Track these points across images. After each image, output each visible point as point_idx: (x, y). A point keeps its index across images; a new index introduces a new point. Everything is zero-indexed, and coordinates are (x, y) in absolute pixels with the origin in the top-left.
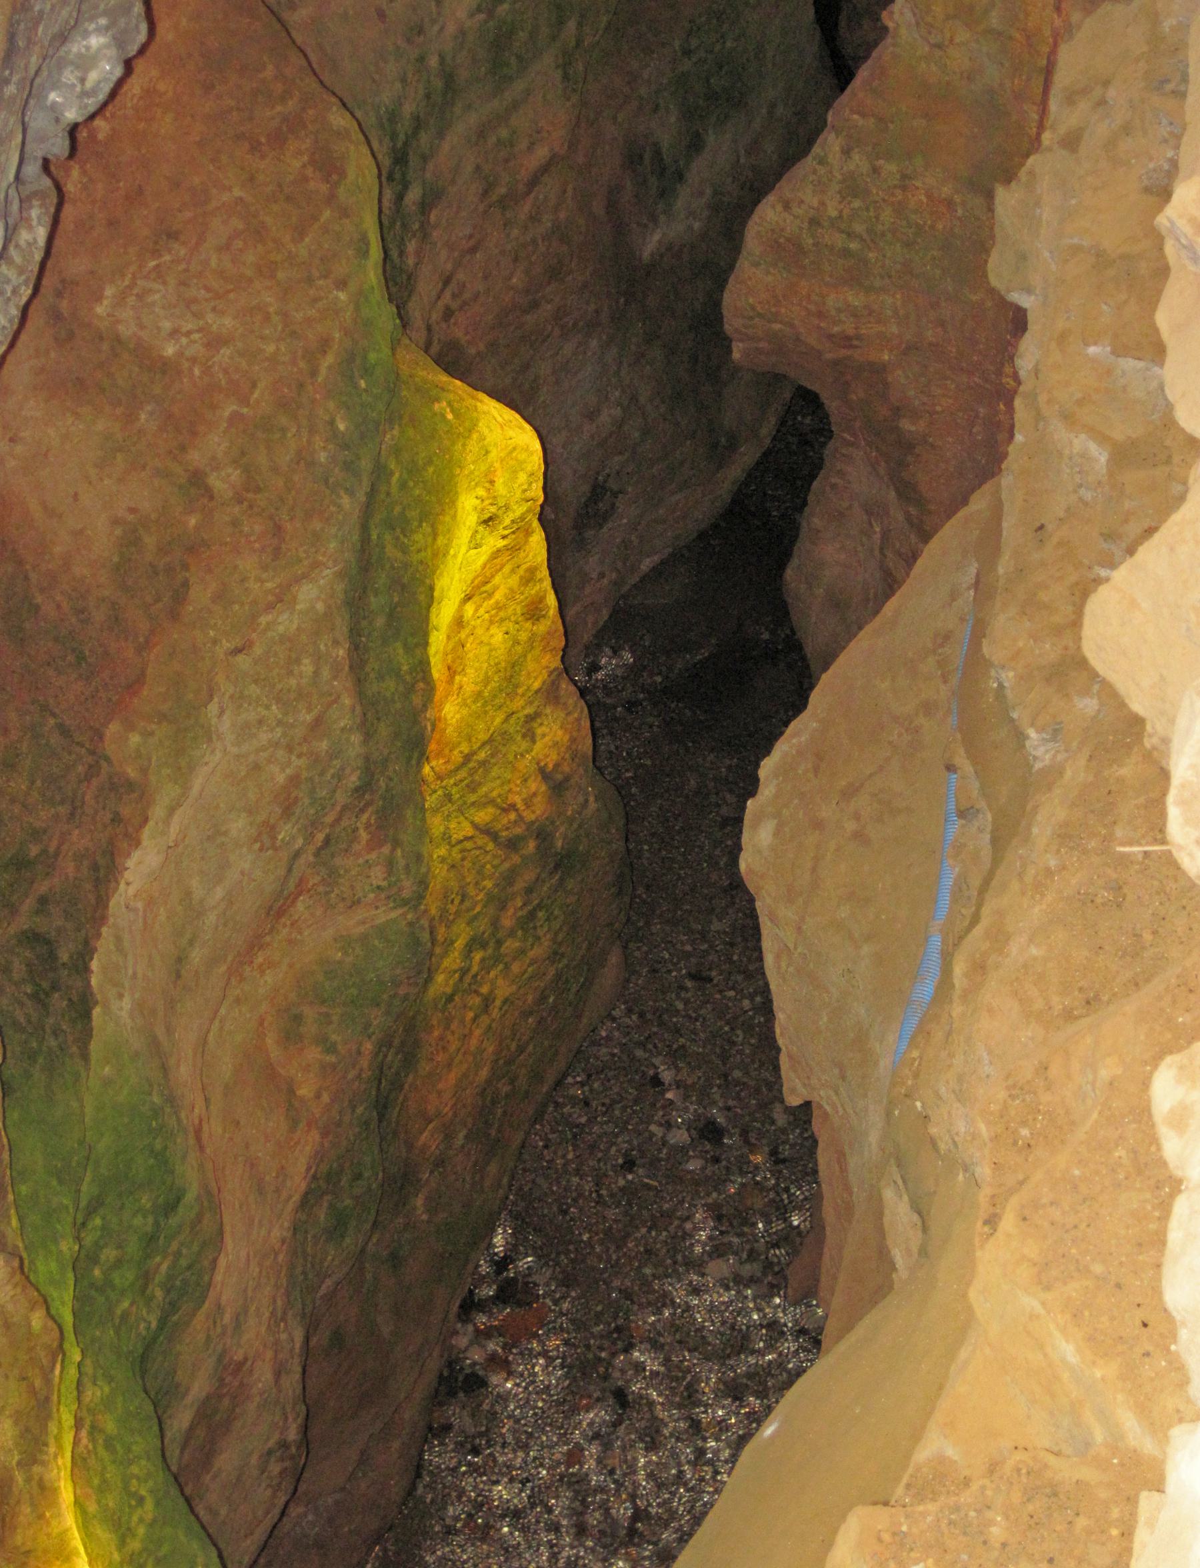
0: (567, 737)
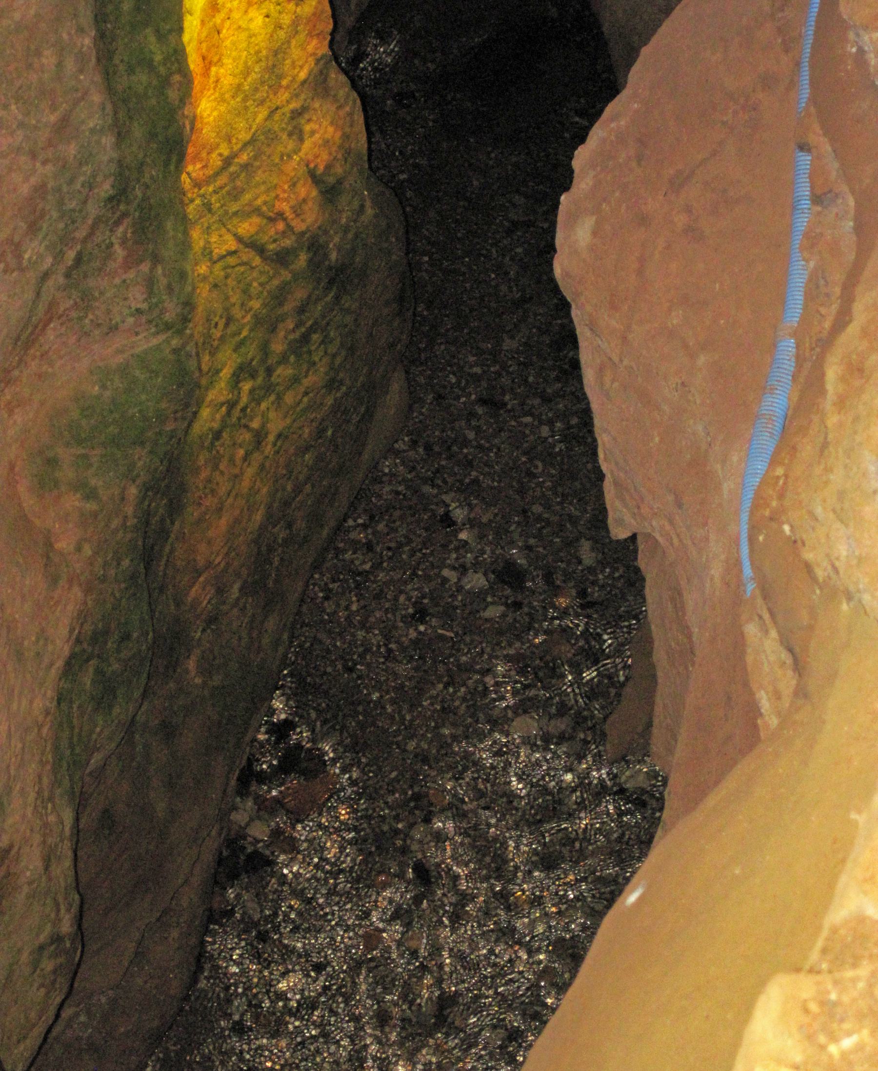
0: (339, 134)
